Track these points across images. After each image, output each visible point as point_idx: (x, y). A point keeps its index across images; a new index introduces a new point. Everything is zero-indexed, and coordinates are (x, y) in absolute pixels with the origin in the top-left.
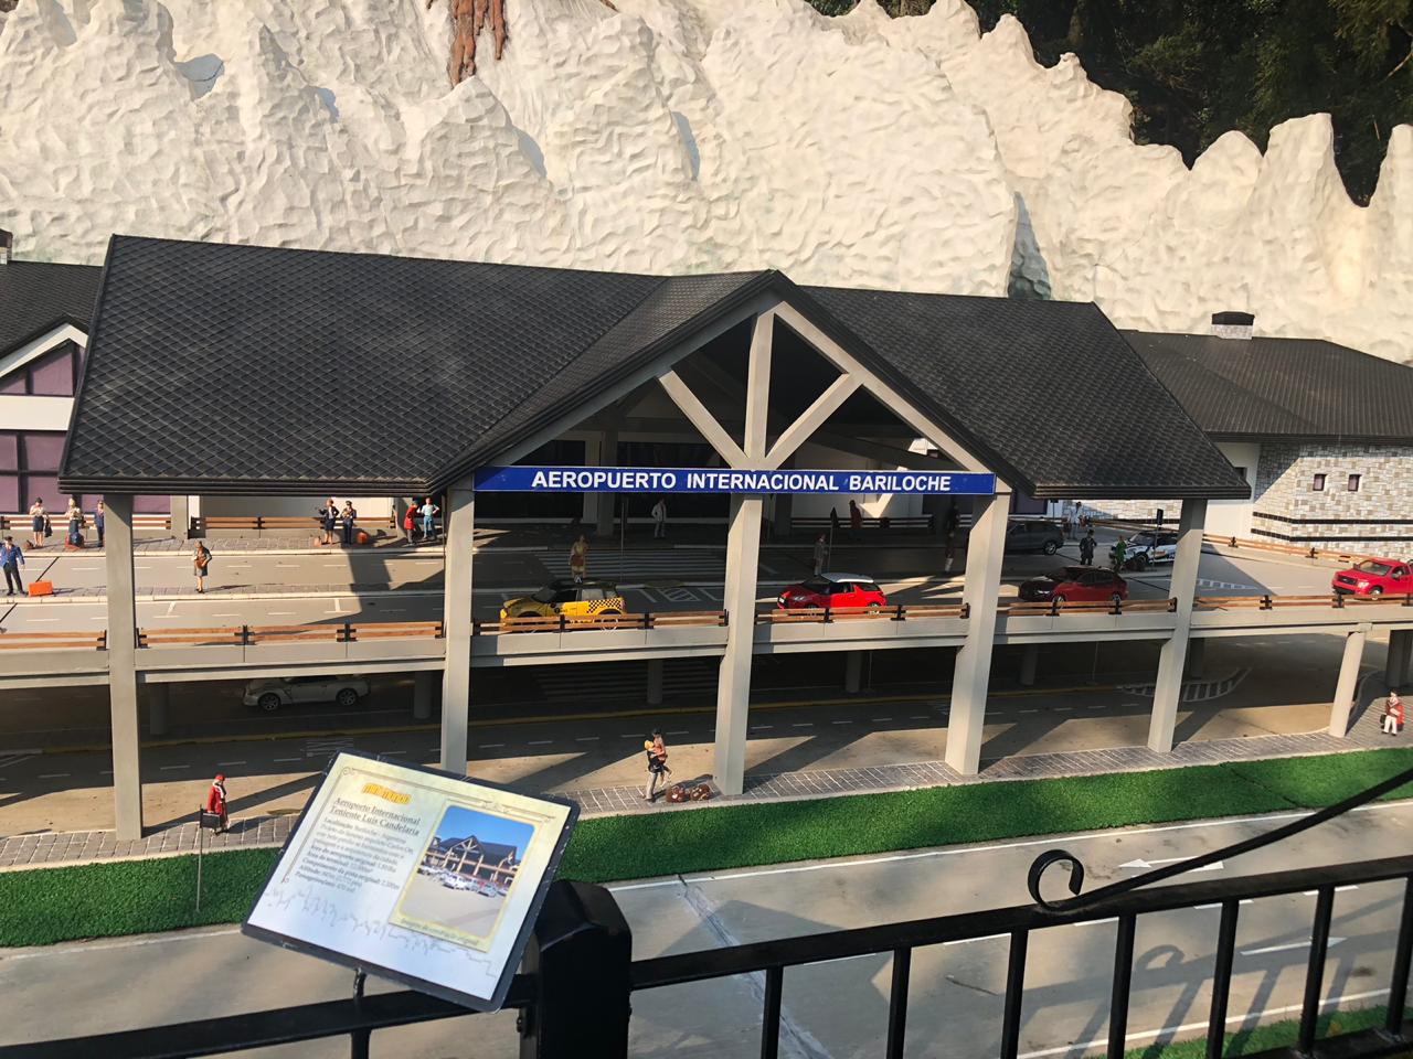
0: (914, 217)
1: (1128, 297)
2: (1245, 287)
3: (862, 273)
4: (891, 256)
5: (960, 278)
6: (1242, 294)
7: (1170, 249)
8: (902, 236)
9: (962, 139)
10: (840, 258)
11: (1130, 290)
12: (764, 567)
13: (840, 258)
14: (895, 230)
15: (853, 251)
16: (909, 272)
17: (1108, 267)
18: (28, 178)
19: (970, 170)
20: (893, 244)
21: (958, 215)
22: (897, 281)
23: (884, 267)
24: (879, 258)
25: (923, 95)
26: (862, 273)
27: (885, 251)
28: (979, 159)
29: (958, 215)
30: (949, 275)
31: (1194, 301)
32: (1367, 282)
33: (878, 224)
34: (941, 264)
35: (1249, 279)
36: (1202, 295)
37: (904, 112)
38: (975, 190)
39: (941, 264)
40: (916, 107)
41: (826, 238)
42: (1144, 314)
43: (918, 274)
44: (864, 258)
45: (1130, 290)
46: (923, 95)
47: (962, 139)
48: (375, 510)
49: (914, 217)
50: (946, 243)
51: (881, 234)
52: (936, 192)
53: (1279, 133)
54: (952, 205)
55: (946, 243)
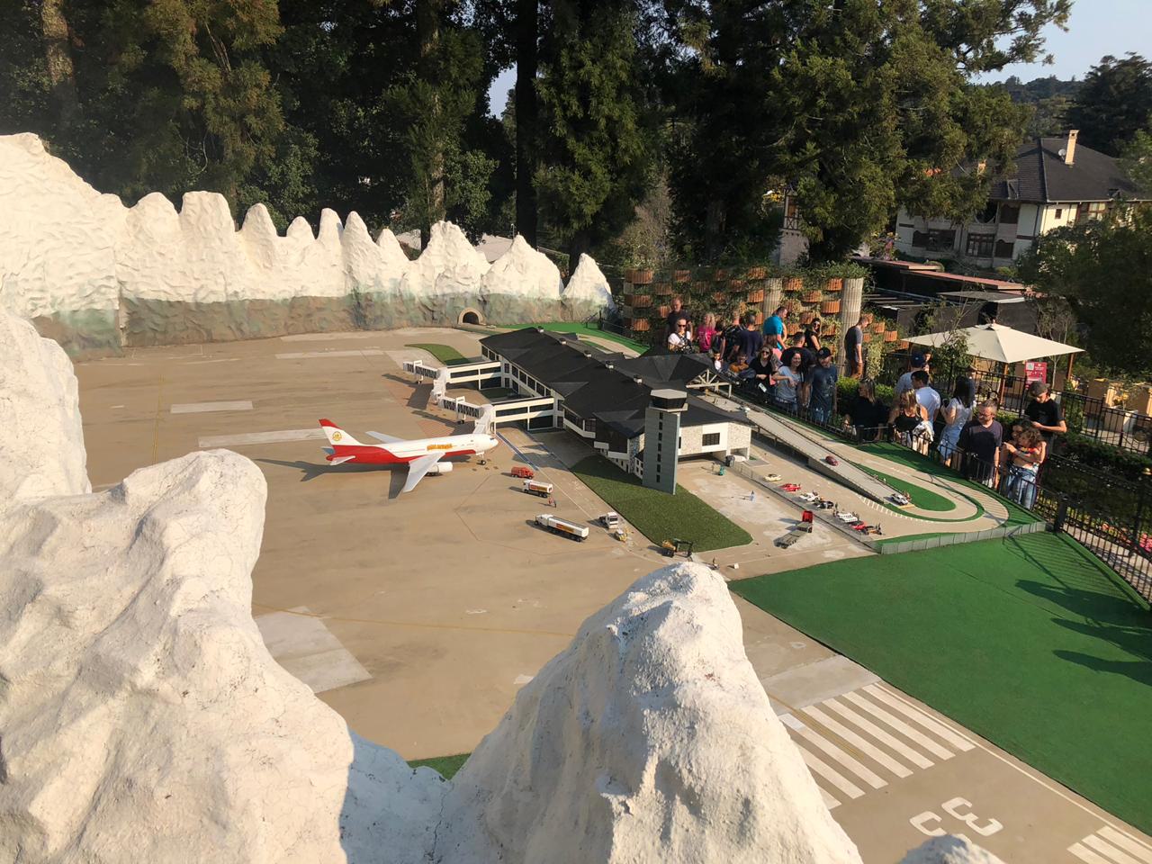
0: (47, 252)
1: (144, 280)
2: (221, 273)
3: (29, 290)
4: (40, 276)
5: (83, 285)
6: (221, 276)
7: (161, 254)
8: (42, 265)
9: (69, 204)
10: (16, 283)
11: (143, 276)
12: (1072, 356)
13: (16, 283)
14: (39, 260)
15: (20, 277)
16: (54, 285)
17: (120, 264)
18: (174, 640)
19: (78, 223)
20: (40, 270)
21: (75, 248)
22: (48, 291)
23: (38, 284)
24: (35, 279)
25: (32, 175)
26: (29, 290)
27: (37, 275)
28: (84, 216)
29: (75, 248)
30: (76, 284)
31: (193, 281)
32: (262, 266)
33: (29, 258)
34: (71, 278)
35: (222, 269)
36: (196, 277)
37: (20, 185)
38: (86, 234)
39: (71, 278)
40: (27, 182)
41: (4, 271)
42: (162, 288)
43: (58, 286)
44: (27, 280)
45: (143, 276)
46: (32, 175)
47: (69, 204)
48: (862, 426)
49: (47, 252)
50: (71, 265)
51: (32, 264)
52: (59, 236)
53: (192, 198)
54: (71, 243)
55: (71, 265)
